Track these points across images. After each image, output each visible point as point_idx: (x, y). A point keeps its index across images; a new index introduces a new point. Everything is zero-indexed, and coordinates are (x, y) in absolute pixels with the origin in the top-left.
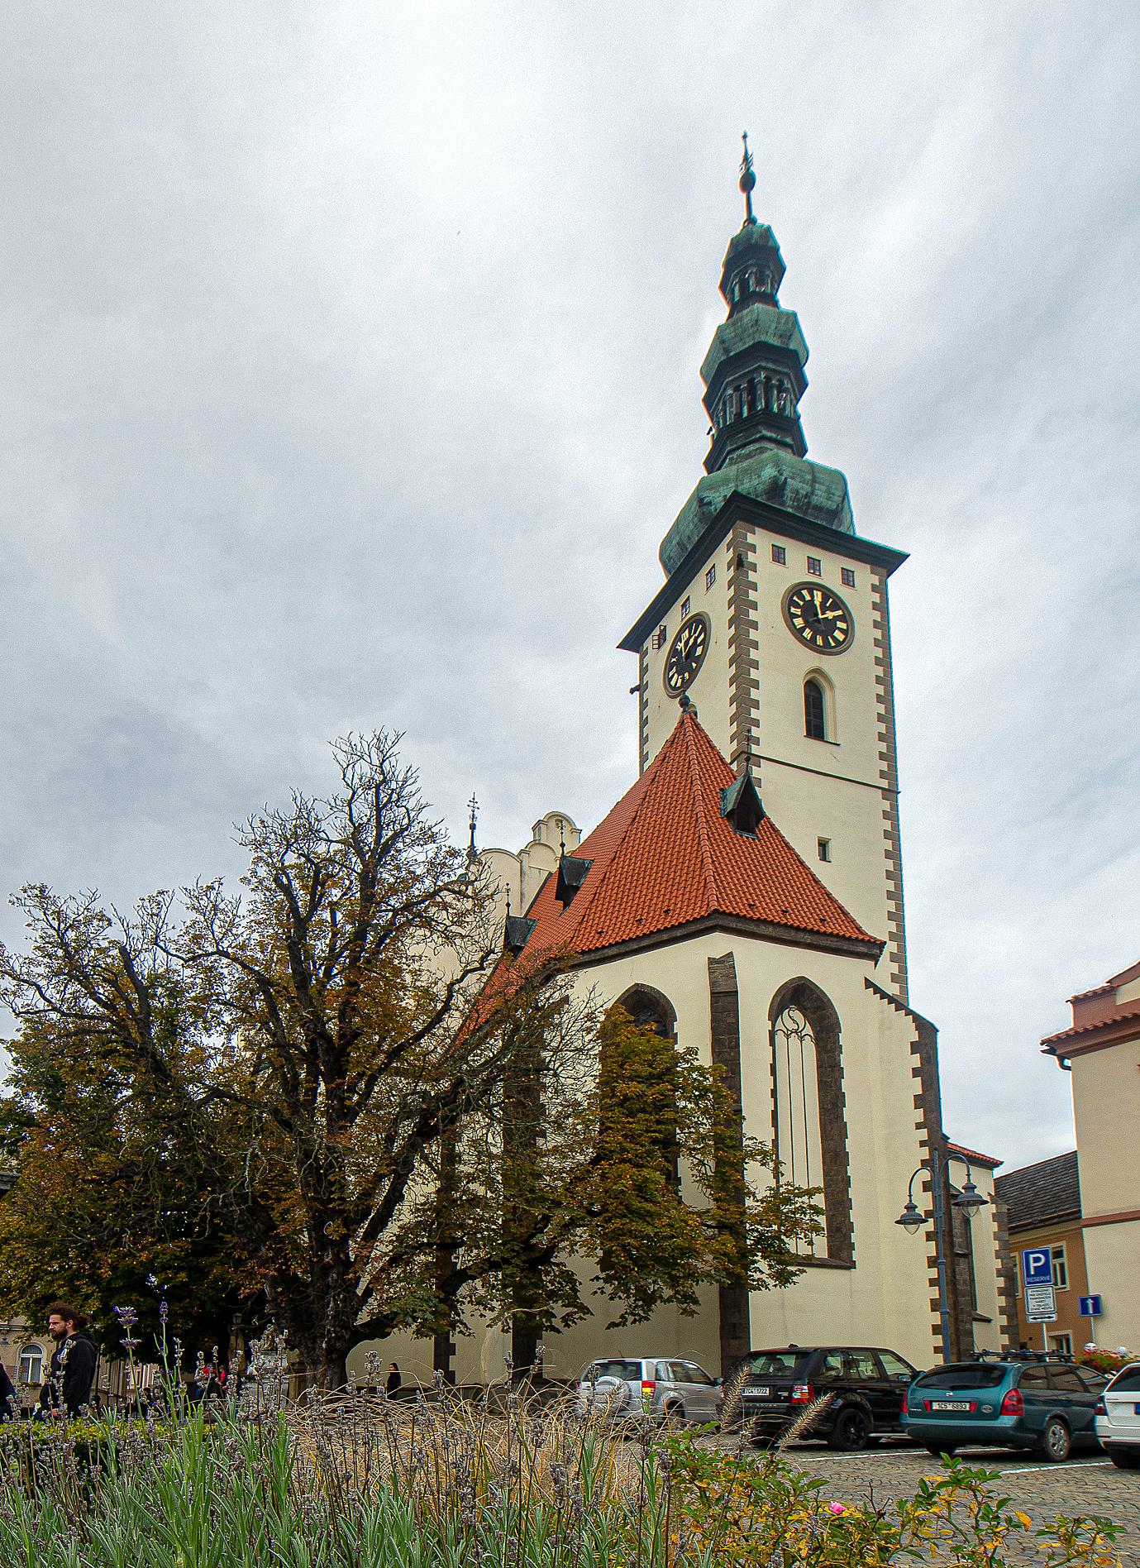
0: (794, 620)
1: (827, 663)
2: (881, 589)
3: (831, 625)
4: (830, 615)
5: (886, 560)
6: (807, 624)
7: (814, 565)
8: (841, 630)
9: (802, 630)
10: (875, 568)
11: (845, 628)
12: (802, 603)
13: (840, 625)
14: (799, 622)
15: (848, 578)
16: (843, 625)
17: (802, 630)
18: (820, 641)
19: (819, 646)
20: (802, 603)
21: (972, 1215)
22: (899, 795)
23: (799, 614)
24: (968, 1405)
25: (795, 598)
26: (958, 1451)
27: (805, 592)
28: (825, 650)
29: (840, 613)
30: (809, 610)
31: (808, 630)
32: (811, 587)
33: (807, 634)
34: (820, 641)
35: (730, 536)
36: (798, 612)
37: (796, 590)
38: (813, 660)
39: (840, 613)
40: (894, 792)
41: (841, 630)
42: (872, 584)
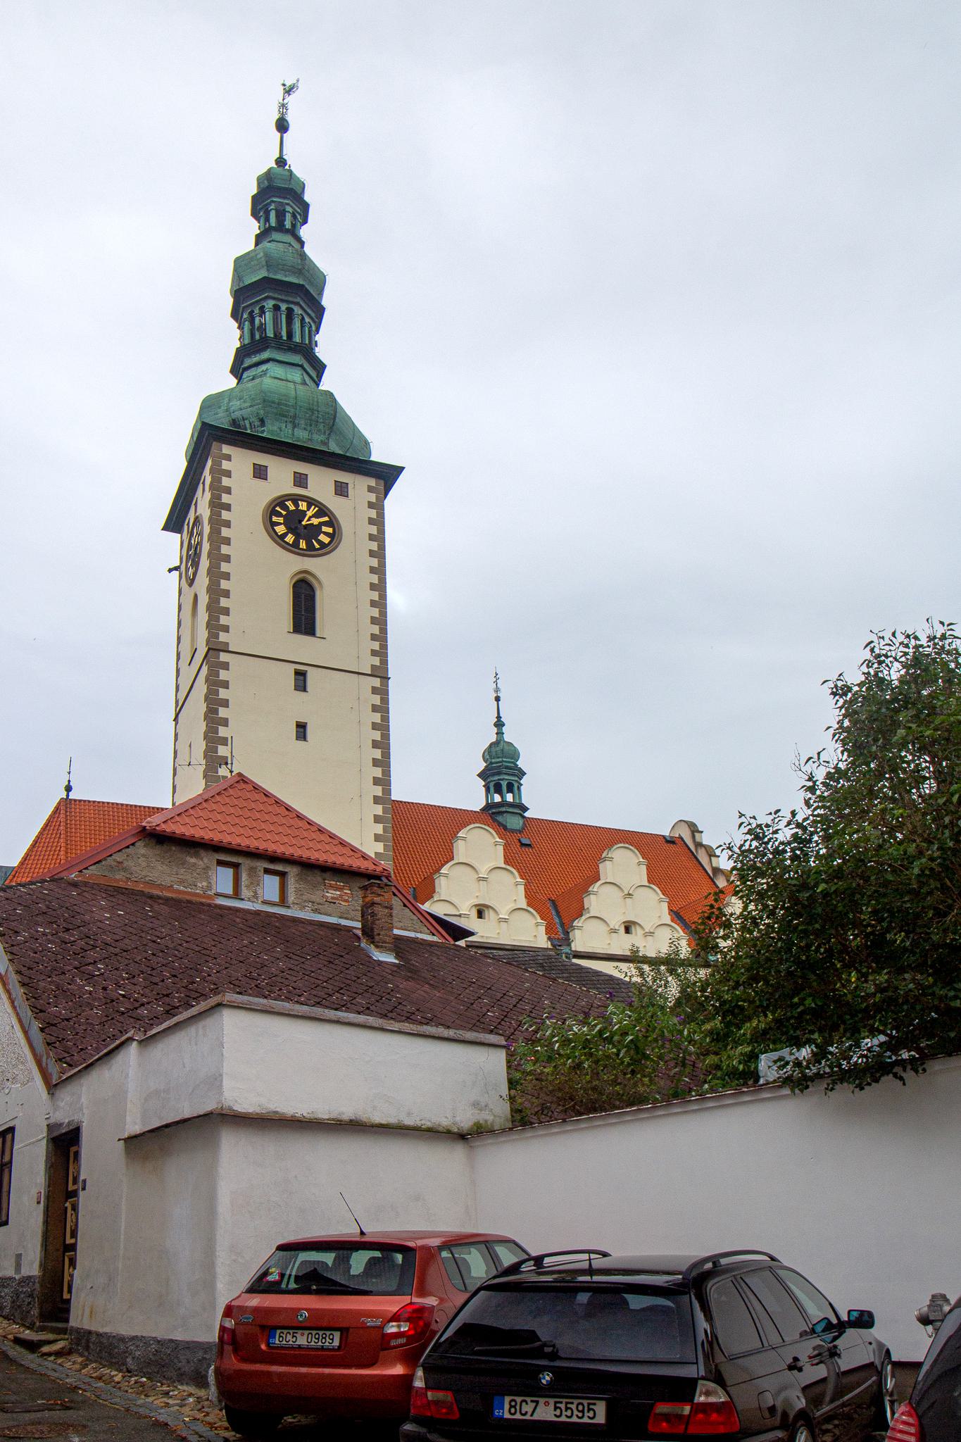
0: (275, 528)
1: (310, 564)
2: (378, 506)
3: (317, 530)
4: (315, 521)
5: (387, 476)
6: (291, 530)
7: (300, 480)
8: (326, 534)
9: (285, 535)
10: (299, 191)
11: (328, 519)
12: (284, 513)
13: (324, 529)
14: (281, 529)
15: (341, 490)
16: (330, 530)
17: (285, 535)
18: (303, 544)
19: (302, 549)
20: (284, 513)
21: (33, 1019)
22: (390, 681)
23: (282, 522)
24: (337, 1335)
25: (278, 509)
26: (289, 1419)
27: (289, 503)
28: (311, 551)
29: (326, 519)
30: (294, 520)
31: (290, 536)
32: (295, 499)
33: (290, 538)
34: (303, 544)
35: (209, 463)
36: (281, 520)
37: (281, 501)
38: (295, 564)
39: (326, 519)
40: (385, 678)
41: (326, 534)
42: (369, 502)
